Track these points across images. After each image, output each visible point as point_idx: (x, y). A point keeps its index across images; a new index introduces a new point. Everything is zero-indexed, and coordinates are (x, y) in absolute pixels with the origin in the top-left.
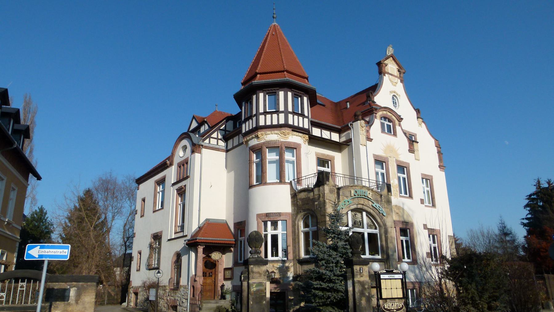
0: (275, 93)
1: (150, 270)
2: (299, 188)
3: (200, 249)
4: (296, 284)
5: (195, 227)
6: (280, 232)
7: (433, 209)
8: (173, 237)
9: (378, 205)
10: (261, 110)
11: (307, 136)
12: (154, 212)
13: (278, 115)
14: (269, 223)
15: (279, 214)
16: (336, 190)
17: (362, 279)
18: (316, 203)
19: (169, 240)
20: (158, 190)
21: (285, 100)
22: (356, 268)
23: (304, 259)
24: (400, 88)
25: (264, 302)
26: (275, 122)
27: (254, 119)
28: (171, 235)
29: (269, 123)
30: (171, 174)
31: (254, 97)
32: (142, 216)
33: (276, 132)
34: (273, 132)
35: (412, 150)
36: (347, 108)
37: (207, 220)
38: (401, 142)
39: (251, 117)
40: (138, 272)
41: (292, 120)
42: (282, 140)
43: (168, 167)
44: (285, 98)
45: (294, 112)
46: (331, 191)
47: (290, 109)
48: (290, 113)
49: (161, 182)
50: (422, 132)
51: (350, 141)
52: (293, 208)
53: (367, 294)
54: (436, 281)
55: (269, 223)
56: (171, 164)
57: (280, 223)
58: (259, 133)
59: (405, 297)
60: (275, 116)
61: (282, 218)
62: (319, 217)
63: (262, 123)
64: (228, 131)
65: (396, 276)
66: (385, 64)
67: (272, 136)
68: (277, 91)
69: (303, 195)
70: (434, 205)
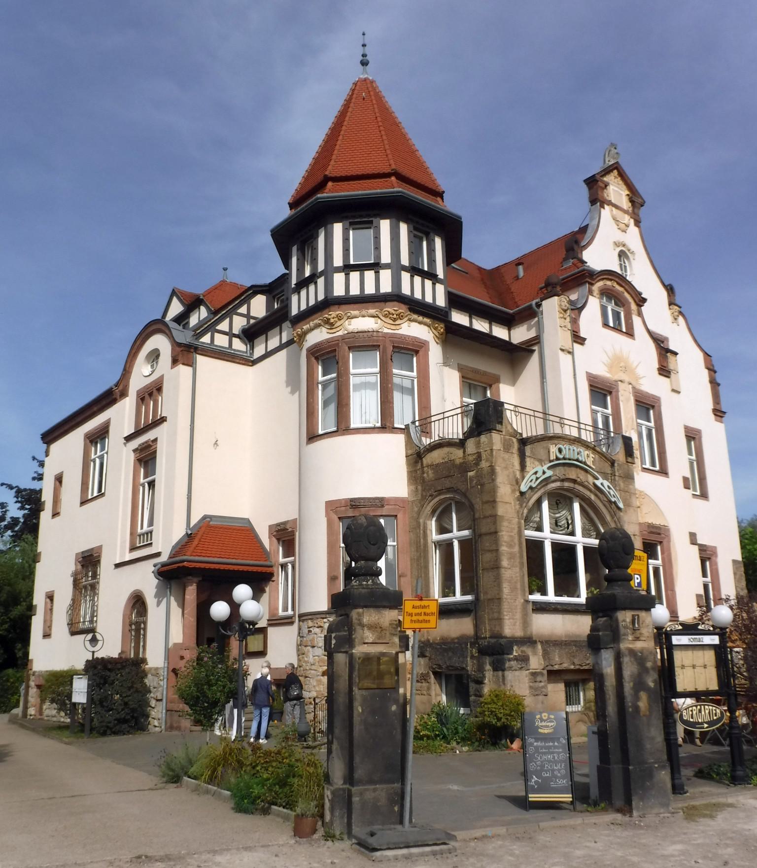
0: (371, 222)
1: (73, 633)
2: (426, 441)
3: (191, 592)
5: (178, 532)
7: (700, 502)
8: (127, 559)
9: (606, 483)
10: (338, 261)
12: (83, 503)
13: (377, 273)
16: (516, 445)
17: (639, 645)
18: (470, 474)
19: (118, 566)
20: (93, 457)
21: (392, 239)
22: (625, 617)
24: (633, 238)
25: (394, 708)
26: (370, 290)
27: (321, 281)
28: (123, 554)
29: (355, 291)
30: (122, 416)
32: (55, 514)
33: (372, 311)
34: (364, 312)
35: (664, 371)
37: (205, 517)
38: (642, 354)
39: (313, 278)
40: (47, 640)
42: (386, 331)
44: (390, 237)
46: (507, 447)
48: (404, 268)
49: (99, 436)
50: (679, 337)
51: (537, 340)
52: (413, 487)
54: (655, 662)
56: (124, 394)
58: (332, 314)
60: (370, 275)
62: (477, 503)
64: (254, 318)
66: (603, 182)
67: (363, 322)
68: (375, 220)
69: (436, 457)
70: (704, 495)
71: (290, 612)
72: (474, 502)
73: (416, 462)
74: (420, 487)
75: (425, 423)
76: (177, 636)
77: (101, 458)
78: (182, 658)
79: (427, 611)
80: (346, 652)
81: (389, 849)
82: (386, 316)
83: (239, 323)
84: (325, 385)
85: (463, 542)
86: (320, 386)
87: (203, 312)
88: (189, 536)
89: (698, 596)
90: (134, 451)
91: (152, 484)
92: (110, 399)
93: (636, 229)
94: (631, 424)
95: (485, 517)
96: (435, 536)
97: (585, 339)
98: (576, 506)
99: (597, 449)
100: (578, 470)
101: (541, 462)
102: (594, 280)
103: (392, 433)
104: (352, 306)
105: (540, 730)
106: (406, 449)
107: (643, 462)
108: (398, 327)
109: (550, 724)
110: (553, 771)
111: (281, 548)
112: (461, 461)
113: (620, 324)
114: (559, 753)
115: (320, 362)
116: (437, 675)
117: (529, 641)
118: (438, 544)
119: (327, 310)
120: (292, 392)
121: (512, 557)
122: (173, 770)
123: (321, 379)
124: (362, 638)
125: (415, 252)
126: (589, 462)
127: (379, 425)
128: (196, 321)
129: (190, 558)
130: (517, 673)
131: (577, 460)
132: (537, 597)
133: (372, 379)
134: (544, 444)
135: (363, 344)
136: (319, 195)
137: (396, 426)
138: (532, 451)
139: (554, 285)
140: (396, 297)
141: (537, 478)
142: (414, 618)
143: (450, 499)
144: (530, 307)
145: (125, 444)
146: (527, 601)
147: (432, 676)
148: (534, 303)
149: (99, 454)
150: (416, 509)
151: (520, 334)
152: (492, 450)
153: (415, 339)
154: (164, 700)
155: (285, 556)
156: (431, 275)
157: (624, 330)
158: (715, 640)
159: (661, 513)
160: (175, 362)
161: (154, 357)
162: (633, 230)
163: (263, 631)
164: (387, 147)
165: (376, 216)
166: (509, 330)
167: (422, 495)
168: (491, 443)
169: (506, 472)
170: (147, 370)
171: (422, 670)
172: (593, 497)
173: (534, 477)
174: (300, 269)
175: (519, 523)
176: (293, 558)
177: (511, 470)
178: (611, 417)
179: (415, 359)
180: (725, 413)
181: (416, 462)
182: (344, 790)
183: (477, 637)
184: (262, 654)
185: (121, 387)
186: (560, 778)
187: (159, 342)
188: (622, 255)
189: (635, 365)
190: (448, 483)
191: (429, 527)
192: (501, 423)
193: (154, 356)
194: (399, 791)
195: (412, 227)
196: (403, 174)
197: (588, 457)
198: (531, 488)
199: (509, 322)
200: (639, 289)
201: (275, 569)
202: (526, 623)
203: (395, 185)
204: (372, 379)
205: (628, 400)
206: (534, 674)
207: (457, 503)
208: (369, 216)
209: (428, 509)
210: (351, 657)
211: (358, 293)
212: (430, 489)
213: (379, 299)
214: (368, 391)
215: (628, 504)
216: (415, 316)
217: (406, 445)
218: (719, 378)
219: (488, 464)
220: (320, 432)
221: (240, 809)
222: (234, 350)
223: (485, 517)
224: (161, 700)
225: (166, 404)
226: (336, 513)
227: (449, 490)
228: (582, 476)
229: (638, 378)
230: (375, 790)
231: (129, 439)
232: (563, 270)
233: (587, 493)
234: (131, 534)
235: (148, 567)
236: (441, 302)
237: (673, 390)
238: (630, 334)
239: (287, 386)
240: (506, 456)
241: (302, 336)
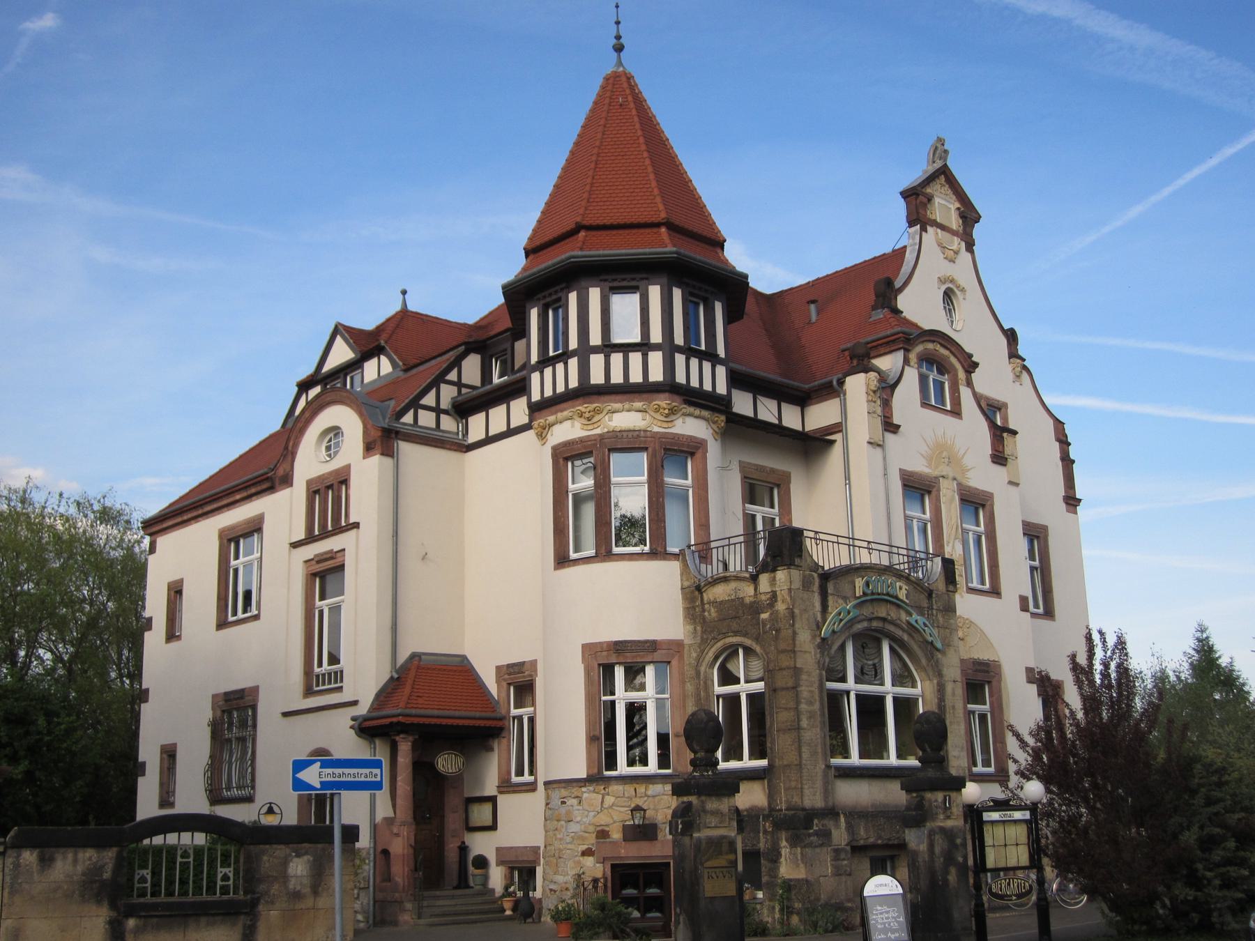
3: (405, 747)
4: (932, 833)
6: (649, 692)
9: (921, 620)
10: (595, 339)
11: (723, 418)
14: (619, 673)
15: (652, 646)
17: (949, 824)
18: (764, 616)
26: (636, 377)
27: (573, 363)
29: (617, 378)
30: (283, 512)
31: (573, 297)
33: (638, 405)
35: (999, 458)
36: (809, 322)
37: (414, 656)
38: (971, 432)
41: (690, 372)
42: (656, 429)
43: (272, 489)
45: (690, 349)
47: (679, 340)
48: (680, 350)
53: (960, 859)
55: (619, 673)
56: (287, 481)
59: (1035, 864)
60: (635, 358)
61: (657, 656)
63: (597, 377)
65: (1018, 815)
66: (925, 195)
67: (626, 418)
68: (641, 284)
69: (720, 592)
70: (1049, 613)
74: (699, 628)
75: (704, 552)
82: (657, 411)
83: (448, 394)
93: (969, 255)
95: (781, 669)
101: (845, 599)
104: (613, 397)
107: (968, 579)
117: (831, 812)
121: (811, 716)
126: (902, 595)
129: (394, 710)
130: (818, 850)
131: (888, 594)
132: (838, 761)
135: (627, 443)
140: (670, 387)
146: (828, 767)
150: (694, 655)
157: (949, 408)
158: (1026, 815)
159: (990, 645)
163: (492, 800)
172: (906, 637)
175: (821, 675)
183: (772, 809)
184: (493, 827)
187: (343, 416)
192: (800, 556)
196: (677, 223)
198: (834, 632)
199: (803, 400)
200: (967, 349)
202: (827, 792)
205: (952, 499)
206: (837, 851)
213: (646, 389)
216: (691, 409)
222: (443, 431)
223: (781, 669)
228: (893, 614)
231: (295, 545)
233: (899, 633)
236: (722, 389)
237: (1011, 483)
238: (956, 412)
240: (805, 595)
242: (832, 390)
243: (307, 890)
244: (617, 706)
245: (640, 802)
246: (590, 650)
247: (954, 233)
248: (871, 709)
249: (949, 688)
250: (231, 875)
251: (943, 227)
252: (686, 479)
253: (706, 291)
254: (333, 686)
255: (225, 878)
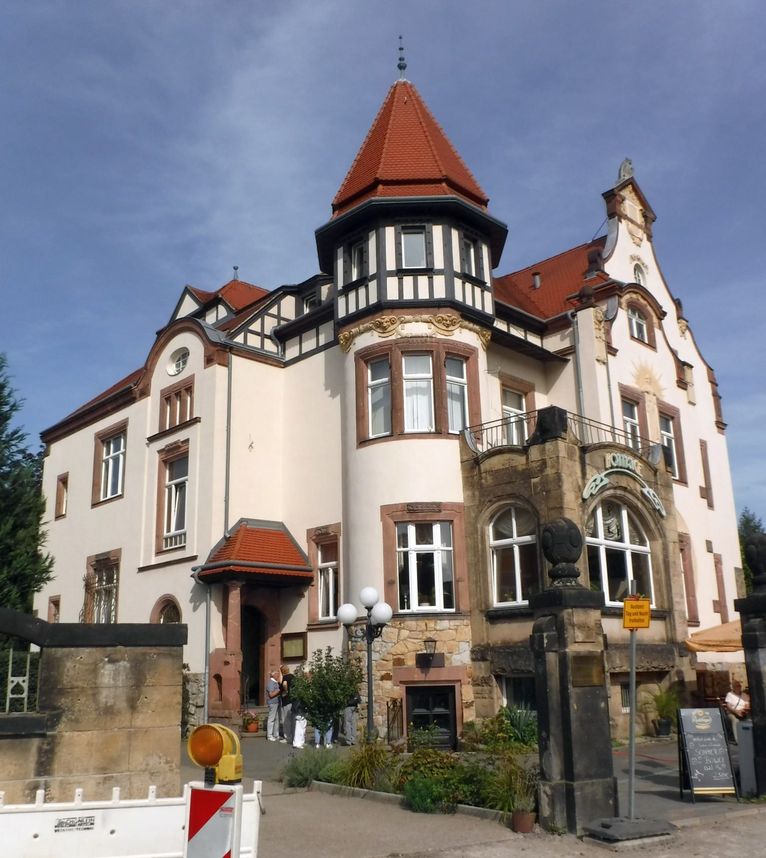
0: (424, 228)
2: (483, 448)
3: (235, 598)
5: (217, 536)
6: (437, 547)
8: (153, 563)
9: (652, 491)
10: (391, 265)
12: (95, 505)
13: (430, 278)
14: (412, 531)
15: (437, 507)
16: (578, 453)
18: (534, 480)
19: (141, 570)
20: (105, 457)
23: (497, 610)
26: (424, 295)
27: (373, 285)
29: (408, 295)
30: (143, 416)
32: (59, 516)
33: (426, 317)
34: (418, 317)
35: (682, 384)
37: (242, 520)
39: (363, 281)
41: (465, 293)
42: (439, 336)
43: (133, 400)
46: (570, 455)
47: (457, 268)
49: (118, 434)
51: (572, 350)
52: (469, 493)
56: (145, 393)
57: (437, 529)
58: (386, 318)
60: (423, 280)
62: (543, 509)
66: (620, 196)
67: (416, 327)
69: (496, 463)
71: (332, 617)
72: (538, 508)
73: (473, 468)
74: (477, 493)
75: (477, 429)
76: (218, 641)
77: (116, 460)
78: (227, 663)
79: (642, 610)
80: (556, 651)
81: (628, 839)
82: (439, 322)
83: (270, 324)
84: (375, 388)
85: (524, 548)
86: (370, 390)
87: (222, 312)
88: (226, 538)
89: (715, 602)
90: (159, 452)
91: (181, 487)
92: (128, 398)
94: (656, 434)
96: (492, 542)
97: (616, 351)
98: (624, 513)
99: (644, 458)
100: (629, 478)
101: (598, 469)
102: (622, 292)
103: (447, 438)
104: (405, 310)
105: (697, 727)
106: (461, 455)
108: (450, 333)
109: (706, 721)
110: (714, 764)
111: (320, 553)
112: (524, 467)
113: (643, 336)
114: (718, 748)
115: (369, 366)
116: (498, 678)
118: (496, 549)
119: (379, 314)
120: (333, 396)
122: (301, 774)
123: (370, 383)
124: (574, 638)
125: (465, 259)
127: (433, 430)
128: (227, 318)
133: (424, 384)
134: (600, 452)
135: (416, 348)
136: (373, 198)
137: (450, 431)
138: (591, 459)
139: (589, 297)
140: (450, 303)
141: (597, 486)
142: (633, 617)
143: (510, 504)
144: (566, 317)
145: (148, 445)
147: (494, 680)
148: (569, 312)
149: (112, 454)
150: (473, 515)
151: (553, 344)
152: (558, 457)
153: (466, 346)
154: (206, 707)
155: (324, 561)
156: (478, 282)
157: (647, 342)
160: (209, 361)
161: (180, 355)
162: (646, 245)
164: (435, 153)
165: (428, 221)
166: (542, 339)
167: (480, 500)
168: (557, 450)
169: (570, 480)
170: (172, 369)
171: (483, 674)
172: (640, 505)
173: (594, 484)
174: (347, 272)
176: (334, 563)
177: (574, 478)
178: (638, 428)
179: (465, 365)
180: (726, 425)
181: (473, 468)
182: (561, 784)
185: (141, 386)
186: (721, 772)
188: (638, 269)
189: (657, 377)
190: (509, 489)
191: (487, 533)
192: (565, 431)
193: (182, 355)
194: (613, 785)
195: (462, 234)
197: (636, 466)
198: (592, 495)
199: (542, 331)
200: (661, 303)
201: (314, 573)
203: (447, 191)
204: (424, 384)
205: (653, 411)
207: (516, 509)
208: (421, 221)
209: (487, 514)
210: (563, 658)
211: (412, 298)
212: (489, 495)
214: (419, 396)
215: (668, 513)
216: (466, 323)
217: (461, 451)
218: (720, 390)
219: (554, 471)
220: (371, 436)
221: (409, 805)
224: (202, 706)
225: (199, 405)
226: (392, 517)
227: (510, 496)
228: (632, 485)
229: (660, 390)
230: (593, 784)
231: (152, 439)
232: (584, 281)
234: (158, 537)
235: (186, 570)
236: (489, 310)
237: (690, 403)
238: (652, 345)
239: (326, 389)
240: (570, 463)
241: (350, 339)
242: (564, 323)
243: (122, 705)
244: (410, 556)
245: (430, 635)
246: (387, 511)
247: (639, 226)
248: (616, 558)
249: (671, 547)
250: (25, 686)
251: (632, 221)
252: (462, 377)
253: (476, 234)
254: (178, 546)
255: (18, 689)
